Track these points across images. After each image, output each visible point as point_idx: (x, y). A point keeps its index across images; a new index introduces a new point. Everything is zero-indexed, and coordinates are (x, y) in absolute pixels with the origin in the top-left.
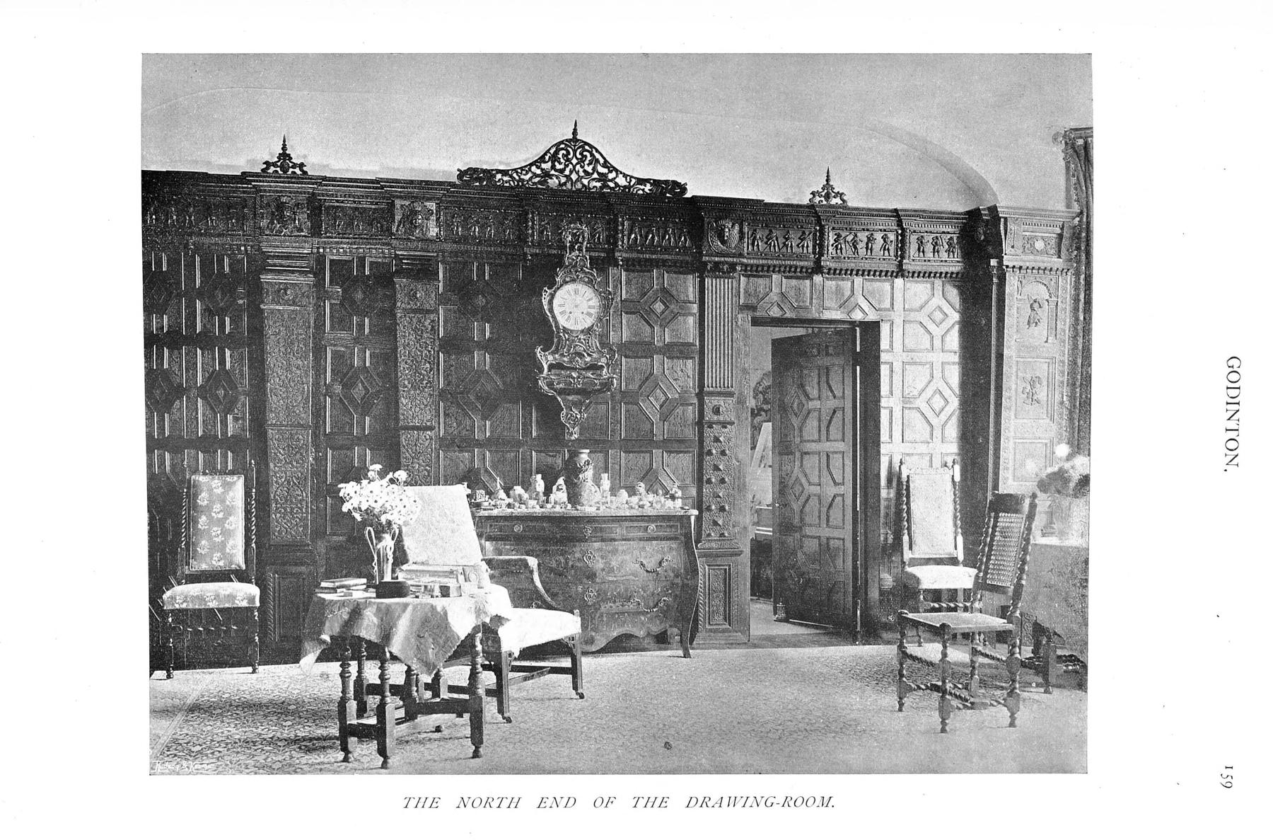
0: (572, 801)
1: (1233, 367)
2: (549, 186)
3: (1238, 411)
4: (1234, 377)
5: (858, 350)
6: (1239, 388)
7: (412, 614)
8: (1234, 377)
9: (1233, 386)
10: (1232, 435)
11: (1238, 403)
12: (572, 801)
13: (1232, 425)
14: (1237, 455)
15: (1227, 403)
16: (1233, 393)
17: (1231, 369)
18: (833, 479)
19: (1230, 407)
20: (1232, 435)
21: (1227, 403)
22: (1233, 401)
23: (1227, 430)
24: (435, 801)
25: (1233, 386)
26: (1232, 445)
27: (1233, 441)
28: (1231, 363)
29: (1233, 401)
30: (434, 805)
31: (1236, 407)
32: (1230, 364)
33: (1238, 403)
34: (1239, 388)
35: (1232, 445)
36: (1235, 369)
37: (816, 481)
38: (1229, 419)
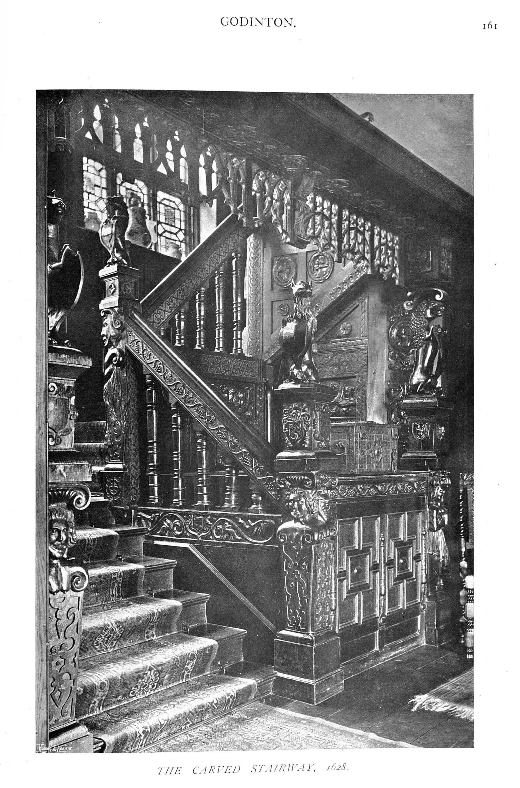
0: (237, 768)
1: (228, 22)
2: (108, 217)
3: (256, 19)
4: (234, 21)
5: (269, 441)
6: (241, 18)
7: (142, 653)
8: (234, 21)
9: (240, 21)
10: (272, 22)
11: (251, 18)
12: (237, 768)
13: (265, 22)
14: (256, 19)
15: (251, 25)
16: (244, 22)
17: (229, 23)
18: (166, 199)
19: (253, 24)
20: (272, 22)
21: (251, 25)
22: (250, 22)
23: (269, 26)
24: (179, 769)
25: (240, 21)
26: (278, 22)
27: (223, 21)
28: (225, 23)
29: (250, 22)
30: (178, 772)
31: (254, 20)
32: (226, 24)
33: (251, 18)
34: (241, 18)
35: (278, 22)
36: (229, 20)
37: (163, 202)
38: (262, 24)
